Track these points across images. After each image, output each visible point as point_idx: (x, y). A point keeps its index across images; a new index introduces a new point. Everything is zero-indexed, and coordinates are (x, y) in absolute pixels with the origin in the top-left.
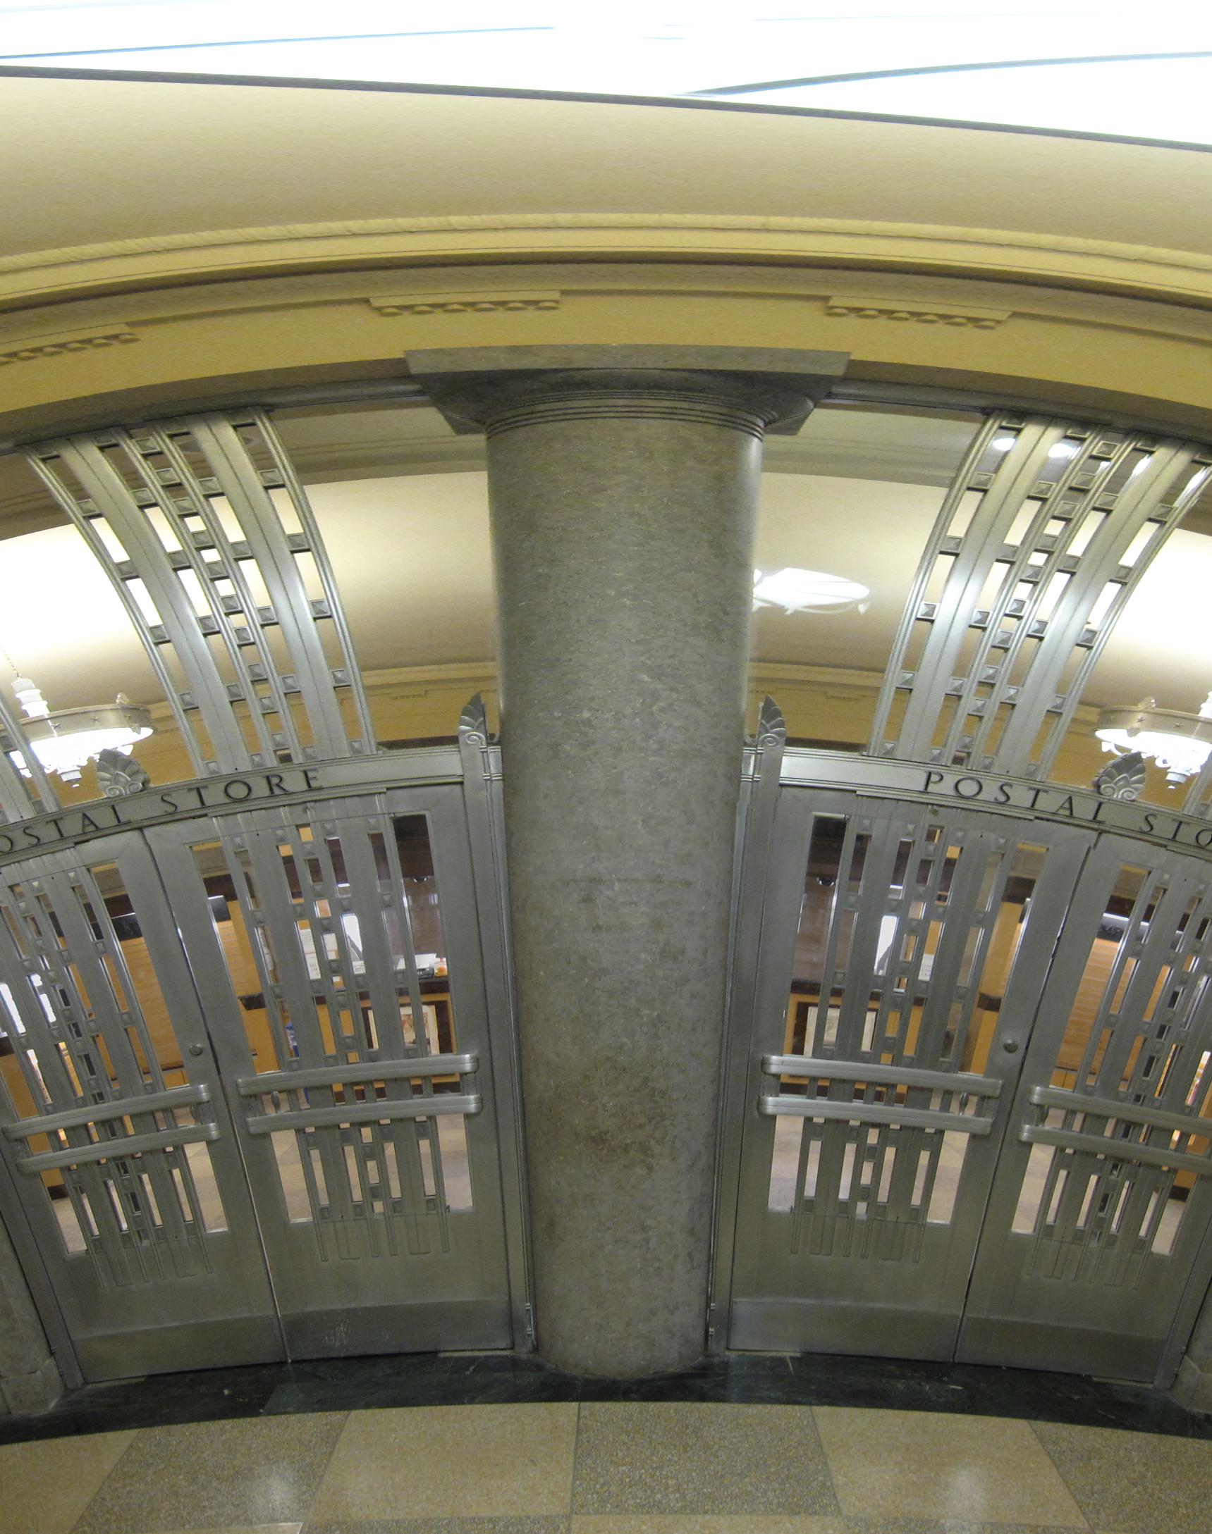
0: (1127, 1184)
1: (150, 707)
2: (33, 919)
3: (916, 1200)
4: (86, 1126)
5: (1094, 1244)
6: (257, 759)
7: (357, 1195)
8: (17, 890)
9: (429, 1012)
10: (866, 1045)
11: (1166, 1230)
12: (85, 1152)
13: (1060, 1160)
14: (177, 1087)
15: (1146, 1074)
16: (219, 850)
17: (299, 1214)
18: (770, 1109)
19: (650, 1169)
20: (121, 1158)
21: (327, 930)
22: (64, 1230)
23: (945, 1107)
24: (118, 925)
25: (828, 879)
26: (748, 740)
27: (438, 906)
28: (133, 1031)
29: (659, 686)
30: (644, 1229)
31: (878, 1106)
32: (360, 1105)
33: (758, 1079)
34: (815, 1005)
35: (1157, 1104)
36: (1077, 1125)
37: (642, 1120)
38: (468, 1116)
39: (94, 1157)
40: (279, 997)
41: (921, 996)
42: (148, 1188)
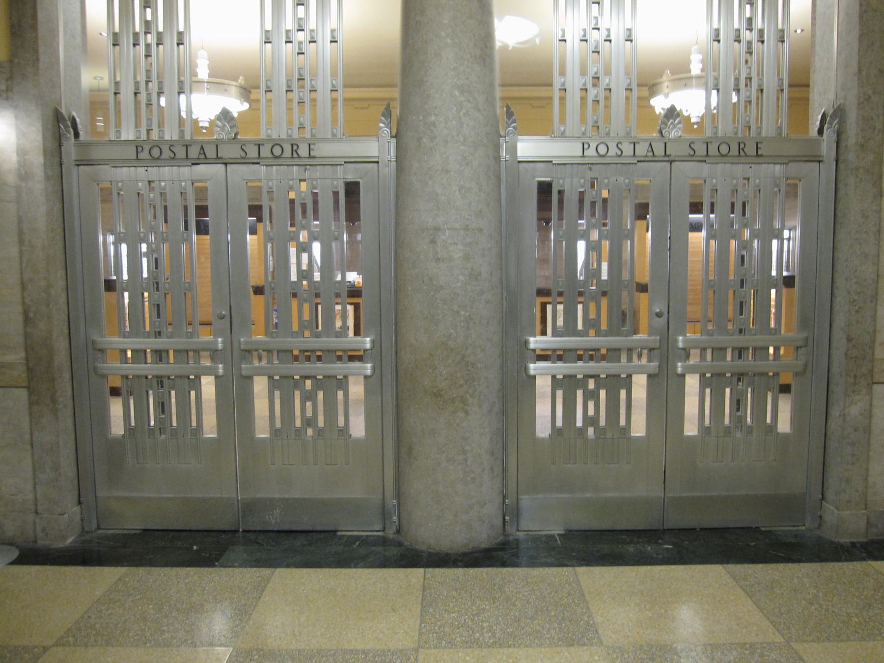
0: (749, 390)
2: (154, 207)
3: (622, 422)
4: (145, 351)
5: (739, 435)
6: (290, 131)
7: (298, 423)
8: (153, 185)
9: (350, 309)
10: (580, 326)
11: (784, 416)
12: (140, 368)
13: (704, 383)
14: (205, 337)
15: (741, 314)
16: (260, 188)
17: (262, 432)
18: (532, 372)
19: (467, 413)
20: (161, 377)
21: (304, 250)
22: (112, 418)
23: (630, 360)
24: (198, 223)
27: (360, 242)
28: (189, 294)
29: (463, 99)
30: (464, 452)
31: (592, 364)
32: (307, 365)
33: (524, 354)
34: (550, 303)
35: (753, 332)
36: (709, 357)
37: (462, 382)
38: (366, 377)
39: (144, 373)
40: (273, 289)
41: (605, 289)
42: (173, 400)
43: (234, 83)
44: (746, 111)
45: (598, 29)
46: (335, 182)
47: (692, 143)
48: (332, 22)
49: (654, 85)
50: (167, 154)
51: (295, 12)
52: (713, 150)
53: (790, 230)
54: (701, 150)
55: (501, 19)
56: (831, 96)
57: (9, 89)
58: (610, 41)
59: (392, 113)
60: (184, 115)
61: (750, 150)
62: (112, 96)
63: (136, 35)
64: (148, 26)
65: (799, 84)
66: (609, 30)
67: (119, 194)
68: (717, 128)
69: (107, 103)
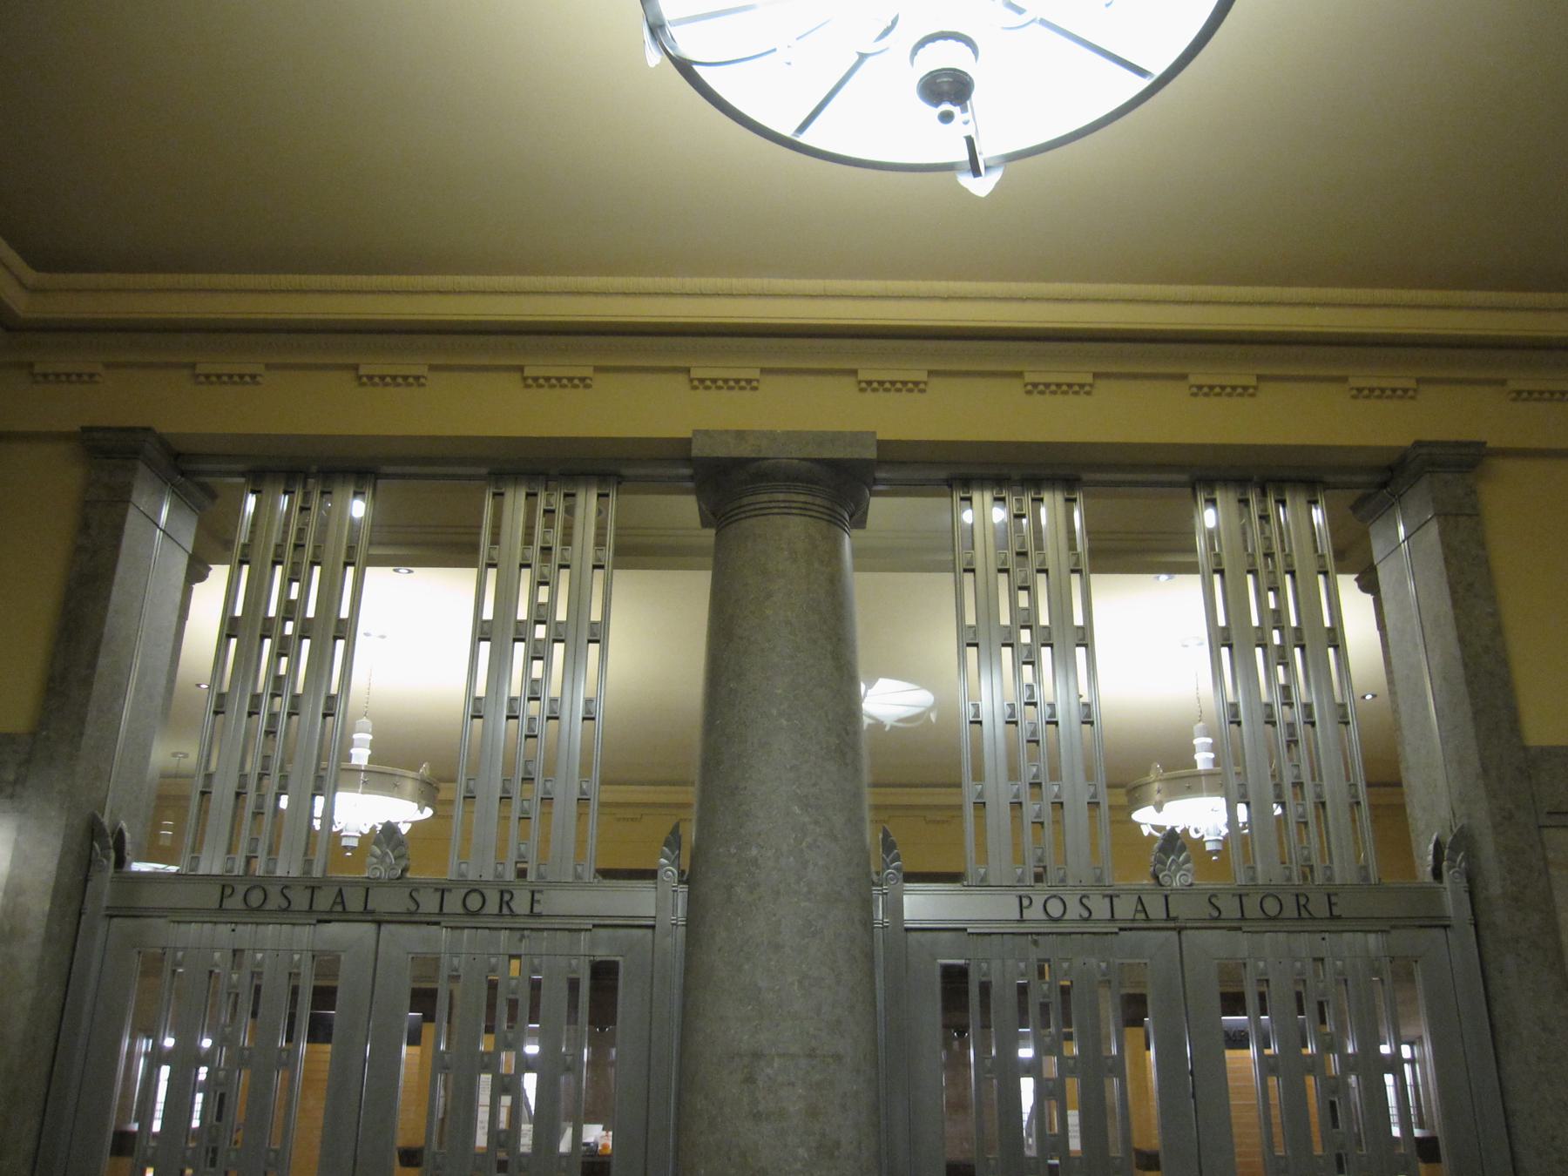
1: (442, 785)
6: (500, 868)
21: (506, 1091)
25: (962, 1030)
26: (875, 878)
27: (612, 1064)
29: (807, 819)
43: (412, 774)
44: (1301, 840)
45: (1035, 704)
46: (574, 962)
47: (1214, 895)
48: (587, 687)
49: (1135, 788)
50: (275, 901)
51: (527, 668)
52: (1252, 909)
53: (1411, 1044)
54: (1230, 908)
55: (870, 685)
56: (1444, 812)
57: (20, 781)
58: (1056, 723)
59: (683, 839)
60: (317, 824)
61: (1319, 907)
62: (196, 797)
63: (256, 698)
64: (278, 683)
65: (1384, 782)
66: (1052, 706)
67: (174, 971)
68: (1253, 868)
69: (187, 798)
